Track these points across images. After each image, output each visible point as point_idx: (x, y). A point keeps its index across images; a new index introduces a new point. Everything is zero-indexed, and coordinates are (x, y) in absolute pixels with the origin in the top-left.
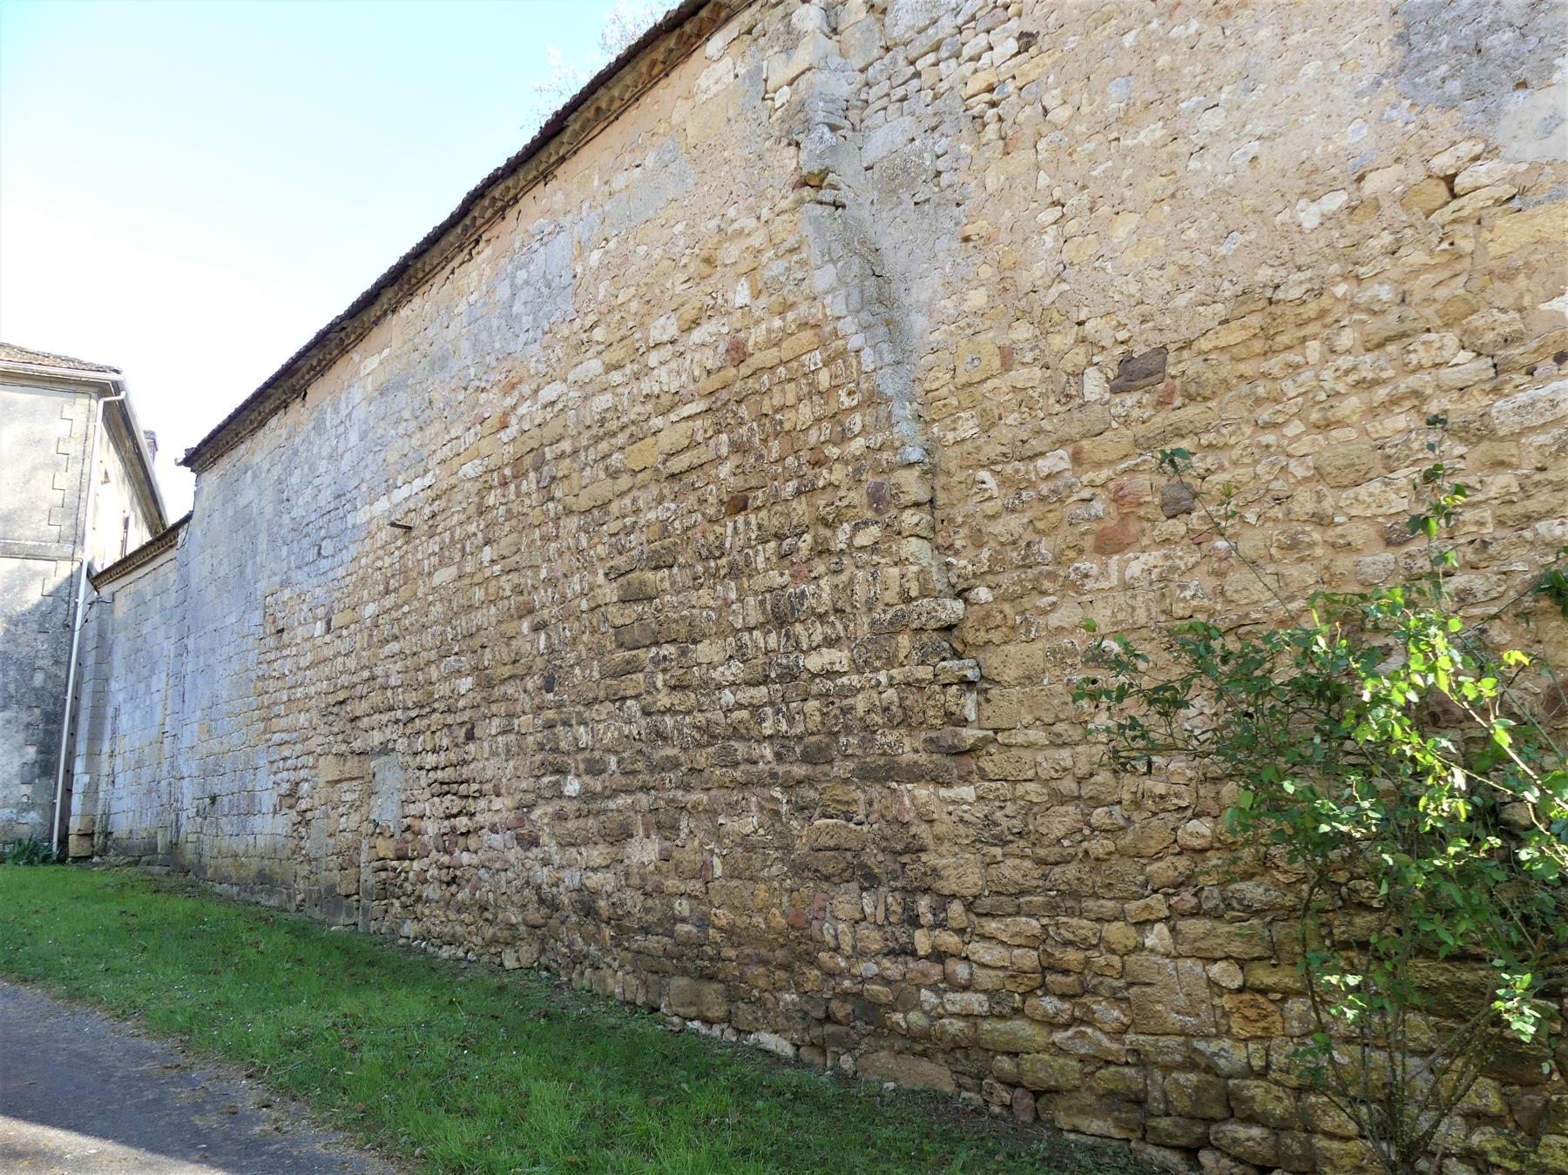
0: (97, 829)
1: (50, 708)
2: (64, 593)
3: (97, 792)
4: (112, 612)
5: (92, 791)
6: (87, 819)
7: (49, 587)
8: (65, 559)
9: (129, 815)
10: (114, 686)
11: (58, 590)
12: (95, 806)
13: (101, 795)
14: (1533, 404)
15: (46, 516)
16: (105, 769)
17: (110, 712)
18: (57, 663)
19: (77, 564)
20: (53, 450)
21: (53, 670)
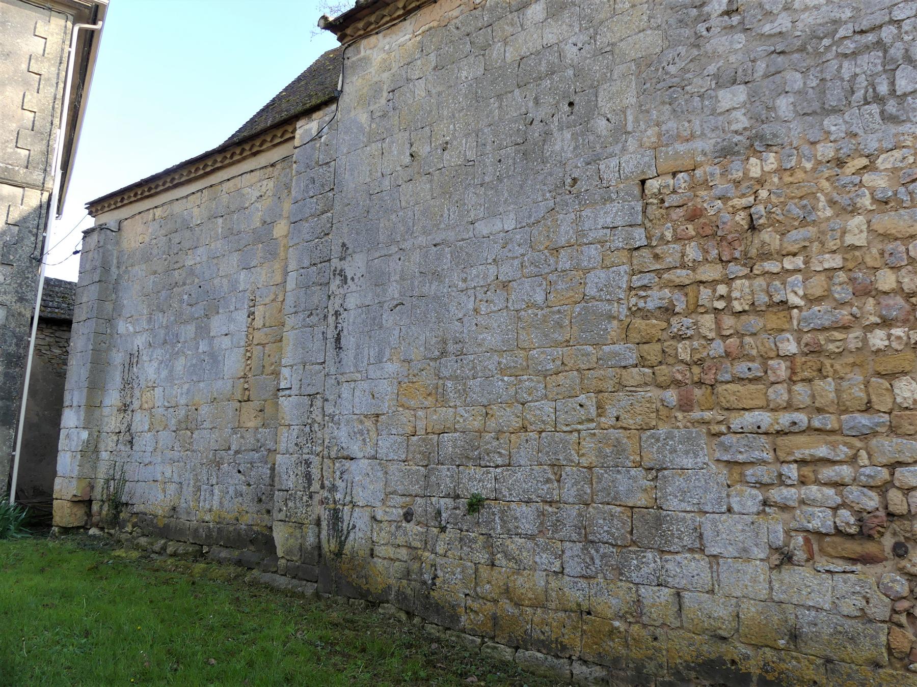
0: (97, 494)
1: (12, 349)
2: (32, 224)
3: (96, 451)
4: (118, 243)
5: (90, 451)
6: (84, 483)
7: (15, 216)
8: (33, 186)
9: (164, 481)
10: (123, 327)
11: (25, 219)
12: (95, 468)
13: (104, 455)
14: (661, 288)
15: (13, 138)
16: (112, 422)
17: (118, 358)
18: (21, 299)
19: (46, 195)
20: (24, 66)
21: (17, 307)
